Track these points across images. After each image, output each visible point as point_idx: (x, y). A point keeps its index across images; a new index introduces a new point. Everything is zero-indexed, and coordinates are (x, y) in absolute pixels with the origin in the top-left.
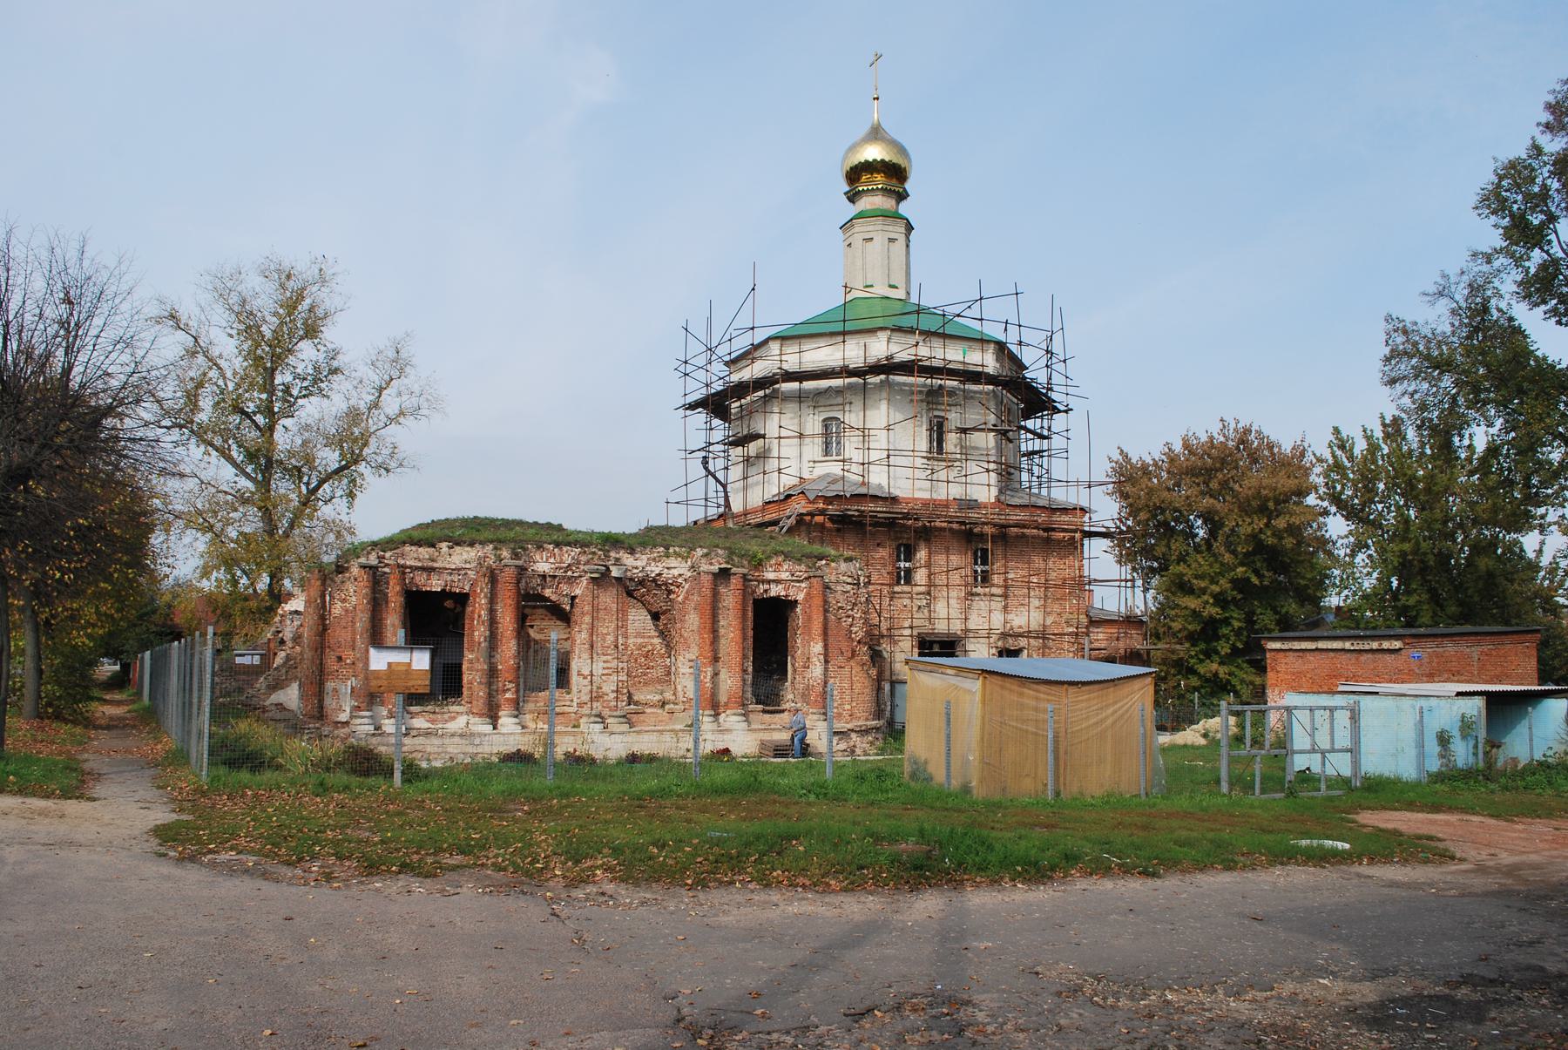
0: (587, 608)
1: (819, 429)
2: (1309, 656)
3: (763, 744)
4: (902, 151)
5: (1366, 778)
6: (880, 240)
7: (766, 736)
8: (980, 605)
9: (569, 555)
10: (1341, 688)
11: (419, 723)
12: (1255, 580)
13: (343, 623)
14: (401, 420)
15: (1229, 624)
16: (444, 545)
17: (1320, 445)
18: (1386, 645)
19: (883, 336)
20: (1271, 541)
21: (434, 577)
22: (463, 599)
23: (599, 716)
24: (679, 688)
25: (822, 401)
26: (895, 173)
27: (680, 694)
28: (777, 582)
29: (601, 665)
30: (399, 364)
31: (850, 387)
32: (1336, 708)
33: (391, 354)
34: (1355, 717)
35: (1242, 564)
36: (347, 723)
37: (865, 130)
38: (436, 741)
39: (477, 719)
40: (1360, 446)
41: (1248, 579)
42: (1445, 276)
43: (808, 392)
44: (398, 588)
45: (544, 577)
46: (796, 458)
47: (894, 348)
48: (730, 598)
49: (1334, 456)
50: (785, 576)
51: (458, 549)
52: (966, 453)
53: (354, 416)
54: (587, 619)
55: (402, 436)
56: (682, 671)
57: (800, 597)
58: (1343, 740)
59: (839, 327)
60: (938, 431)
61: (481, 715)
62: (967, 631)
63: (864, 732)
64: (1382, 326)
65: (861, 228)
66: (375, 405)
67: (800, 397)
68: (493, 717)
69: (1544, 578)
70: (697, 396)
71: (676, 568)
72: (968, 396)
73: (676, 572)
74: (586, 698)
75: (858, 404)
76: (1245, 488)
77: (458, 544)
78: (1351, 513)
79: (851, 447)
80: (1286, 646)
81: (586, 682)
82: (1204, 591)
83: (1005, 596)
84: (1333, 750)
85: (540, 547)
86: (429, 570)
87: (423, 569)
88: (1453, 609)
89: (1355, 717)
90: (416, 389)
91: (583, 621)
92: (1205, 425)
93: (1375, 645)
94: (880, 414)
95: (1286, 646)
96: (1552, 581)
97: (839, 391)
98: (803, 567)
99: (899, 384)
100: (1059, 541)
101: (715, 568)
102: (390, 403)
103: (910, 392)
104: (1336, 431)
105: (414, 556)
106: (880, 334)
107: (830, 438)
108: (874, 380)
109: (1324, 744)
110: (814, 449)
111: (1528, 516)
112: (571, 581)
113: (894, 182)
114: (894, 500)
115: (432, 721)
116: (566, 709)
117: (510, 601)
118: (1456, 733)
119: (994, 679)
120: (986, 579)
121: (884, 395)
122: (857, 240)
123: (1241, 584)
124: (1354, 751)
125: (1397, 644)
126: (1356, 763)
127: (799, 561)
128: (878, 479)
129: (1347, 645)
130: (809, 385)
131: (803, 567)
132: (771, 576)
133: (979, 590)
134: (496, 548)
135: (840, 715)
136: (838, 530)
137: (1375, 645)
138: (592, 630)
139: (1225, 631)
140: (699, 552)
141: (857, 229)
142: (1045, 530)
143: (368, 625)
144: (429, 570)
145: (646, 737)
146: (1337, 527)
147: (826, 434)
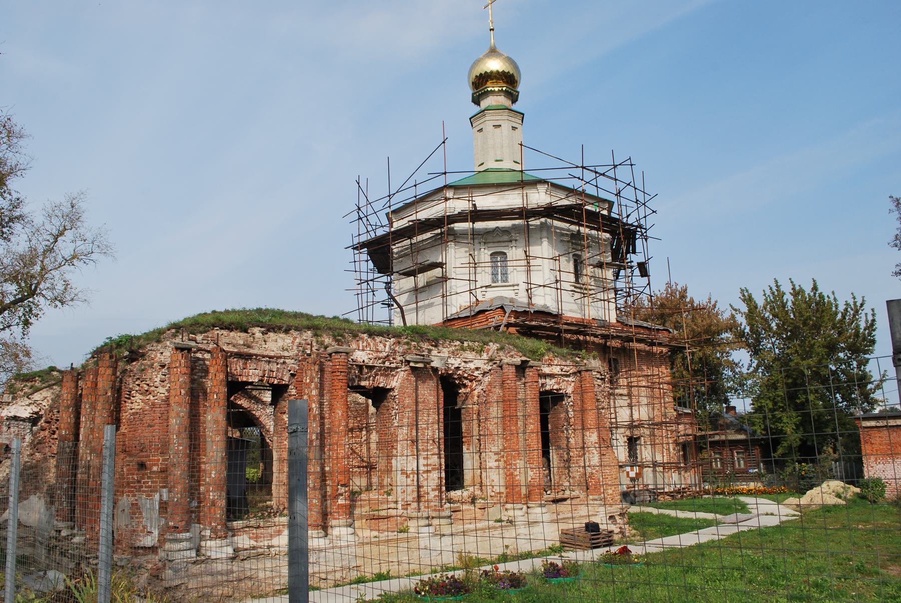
1: (488, 259)
3: (564, 533)
4: (519, 72)
6: (506, 126)
9: (385, 346)
11: (244, 541)
14: (75, 261)
16: (257, 331)
19: (542, 188)
21: (251, 365)
25: (490, 239)
26: (509, 80)
28: (552, 376)
30: (71, 218)
31: (514, 227)
33: (67, 209)
36: (153, 549)
37: (487, 50)
45: (360, 368)
46: (467, 279)
50: (556, 370)
51: (271, 334)
53: (28, 259)
55: (77, 276)
56: (489, 465)
57: (569, 390)
66: (49, 250)
67: (475, 235)
70: (363, 238)
73: (472, 366)
75: (522, 242)
79: (517, 276)
83: (629, 395)
90: (89, 236)
94: (543, 249)
97: (505, 231)
101: (518, 360)
102: (65, 247)
103: (561, 234)
105: (232, 340)
106: (539, 186)
108: (535, 222)
110: (484, 278)
112: (388, 372)
114: (557, 317)
115: (256, 538)
116: (393, 512)
121: (545, 234)
130: (479, 225)
132: (546, 370)
140: (493, 347)
141: (487, 118)
143: (186, 422)
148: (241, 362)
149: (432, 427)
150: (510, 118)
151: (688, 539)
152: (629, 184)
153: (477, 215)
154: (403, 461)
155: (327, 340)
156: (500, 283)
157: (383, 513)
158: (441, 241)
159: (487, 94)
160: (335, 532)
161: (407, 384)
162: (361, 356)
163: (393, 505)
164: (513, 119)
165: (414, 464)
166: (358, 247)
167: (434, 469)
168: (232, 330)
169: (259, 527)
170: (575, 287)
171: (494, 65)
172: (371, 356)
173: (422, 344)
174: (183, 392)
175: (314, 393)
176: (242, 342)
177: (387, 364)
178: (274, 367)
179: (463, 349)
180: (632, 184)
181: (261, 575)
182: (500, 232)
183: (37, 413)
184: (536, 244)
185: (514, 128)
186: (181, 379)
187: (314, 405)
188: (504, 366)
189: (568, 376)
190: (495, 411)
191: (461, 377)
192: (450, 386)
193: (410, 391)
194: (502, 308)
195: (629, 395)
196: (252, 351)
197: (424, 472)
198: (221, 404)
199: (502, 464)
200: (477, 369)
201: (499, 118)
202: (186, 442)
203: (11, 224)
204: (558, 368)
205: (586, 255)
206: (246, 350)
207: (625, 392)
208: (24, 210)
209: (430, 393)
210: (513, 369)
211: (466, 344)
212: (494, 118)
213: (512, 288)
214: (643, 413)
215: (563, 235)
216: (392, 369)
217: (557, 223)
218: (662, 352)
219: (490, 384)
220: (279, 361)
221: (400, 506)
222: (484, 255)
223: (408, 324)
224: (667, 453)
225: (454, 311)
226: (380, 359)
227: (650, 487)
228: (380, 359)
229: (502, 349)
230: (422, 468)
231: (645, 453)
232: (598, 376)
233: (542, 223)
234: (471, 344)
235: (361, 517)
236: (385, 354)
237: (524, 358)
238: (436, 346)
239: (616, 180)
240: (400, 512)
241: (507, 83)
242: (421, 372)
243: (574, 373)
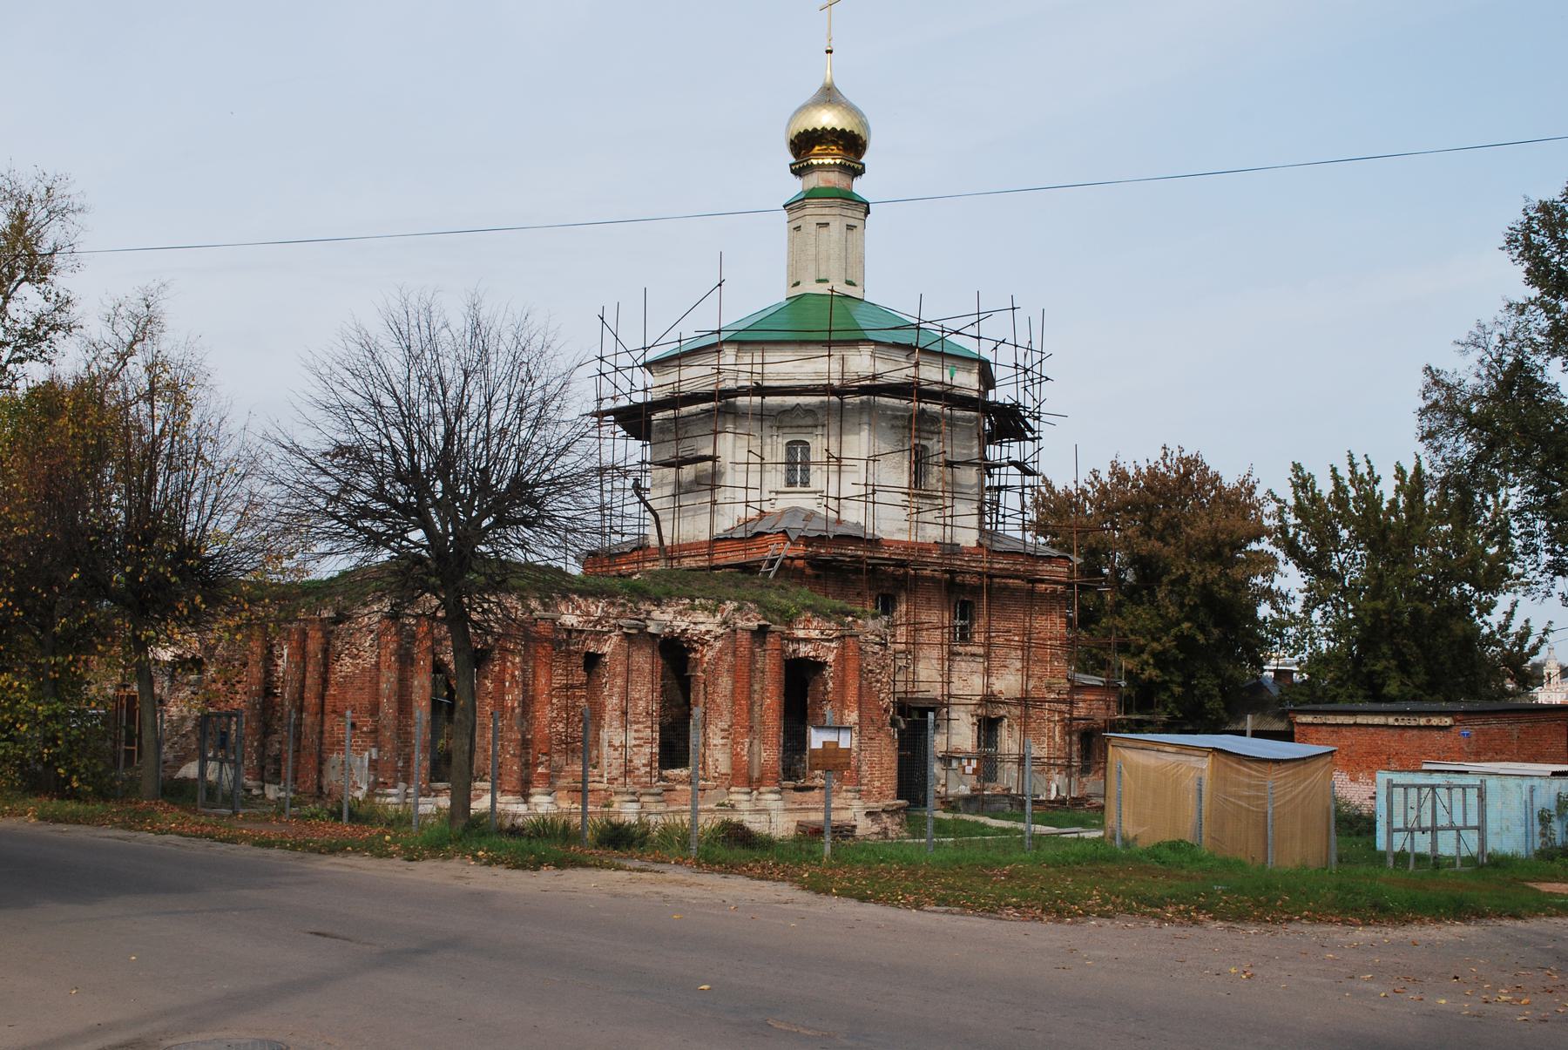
1: (781, 456)
2: (1346, 732)
3: (800, 825)
4: (865, 126)
5: (1489, 856)
6: (837, 226)
7: (802, 817)
8: (961, 666)
10: (1425, 767)
12: (1201, 638)
13: (358, 683)
15: (1167, 689)
17: (1274, 484)
18: (1435, 721)
19: (866, 351)
20: (1224, 593)
24: (710, 761)
26: (851, 144)
28: (807, 641)
29: (633, 734)
31: (822, 406)
32: (1468, 786)
34: (1482, 796)
35: (1187, 619)
37: (814, 89)
39: (510, 798)
40: (1325, 487)
41: (1194, 639)
42: (1481, 327)
43: (771, 409)
45: (569, 631)
46: (751, 485)
47: (881, 367)
49: (1297, 498)
50: (815, 634)
52: (955, 491)
57: (830, 658)
58: (1473, 820)
59: (825, 336)
60: (919, 463)
61: (514, 793)
62: (950, 696)
63: (892, 812)
64: (1421, 380)
65: (814, 213)
67: (762, 415)
69: (1514, 644)
71: (703, 623)
72: (952, 422)
73: (703, 628)
75: (834, 428)
76: (1199, 530)
78: (1304, 562)
80: (1318, 720)
82: (1141, 650)
83: (987, 656)
84: (1466, 828)
85: (565, 597)
88: (1422, 678)
89: (1482, 796)
92: (1141, 453)
93: (1423, 721)
94: (859, 443)
95: (1318, 720)
96: (1522, 648)
97: (809, 411)
98: (833, 624)
99: (887, 407)
100: (1042, 595)
101: (754, 624)
104: (1297, 468)
107: (797, 468)
109: (1459, 822)
110: (776, 478)
111: (1506, 573)
112: (599, 636)
113: (852, 156)
114: (875, 543)
118: (1554, 812)
119: (1221, 758)
120: (965, 638)
121: (865, 418)
122: (809, 224)
123: (1184, 642)
124: (1481, 829)
125: (1448, 721)
126: (1483, 841)
127: (827, 618)
128: (854, 514)
129: (1391, 721)
131: (833, 624)
132: (801, 634)
133: (961, 649)
136: (817, 577)
137: (1423, 721)
138: (625, 695)
139: (1164, 696)
140: (730, 606)
141: (807, 211)
142: (1029, 581)
143: (395, 687)
146: (1291, 580)
147: (791, 464)
149: (645, 696)
154: (611, 733)
155: (534, 604)
156: (798, 488)
160: (534, 800)
161: (619, 650)
162: (570, 619)
164: (850, 213)
165: (626, 739)
171: (827, 119)
173: (641, 605)
179: (694, 609)
182: (798, 418)
183: (179, 656)
184: (851, 432)
185: (850, 227)
190: (725, 683)
191: (689, 641)
192: (675, 655)
193: (622, 658)
194: (784, 532)
195: (987, 656)
199: (728, 741)
200: (708, 632)
201: (827, 211)
202: (395, 705)
203: (52, 334)
205: (934, 445)
207: (981, 651)
208: (75, 312)
209: (644, 660)
210: (748, 635)
212: (819, 211)
214: (1008, 683)
215: (896, 417)
219: (721, 650)
222: (776, 449)
223: (667, 542)
225: (728, 525)
227: (1014, 792)
229: (738, 609)
231: (1008, 742)
233: (862, 402)
238: (658, 606)
240: (604, 786)
241: (845, 149)
242: (636, 637)
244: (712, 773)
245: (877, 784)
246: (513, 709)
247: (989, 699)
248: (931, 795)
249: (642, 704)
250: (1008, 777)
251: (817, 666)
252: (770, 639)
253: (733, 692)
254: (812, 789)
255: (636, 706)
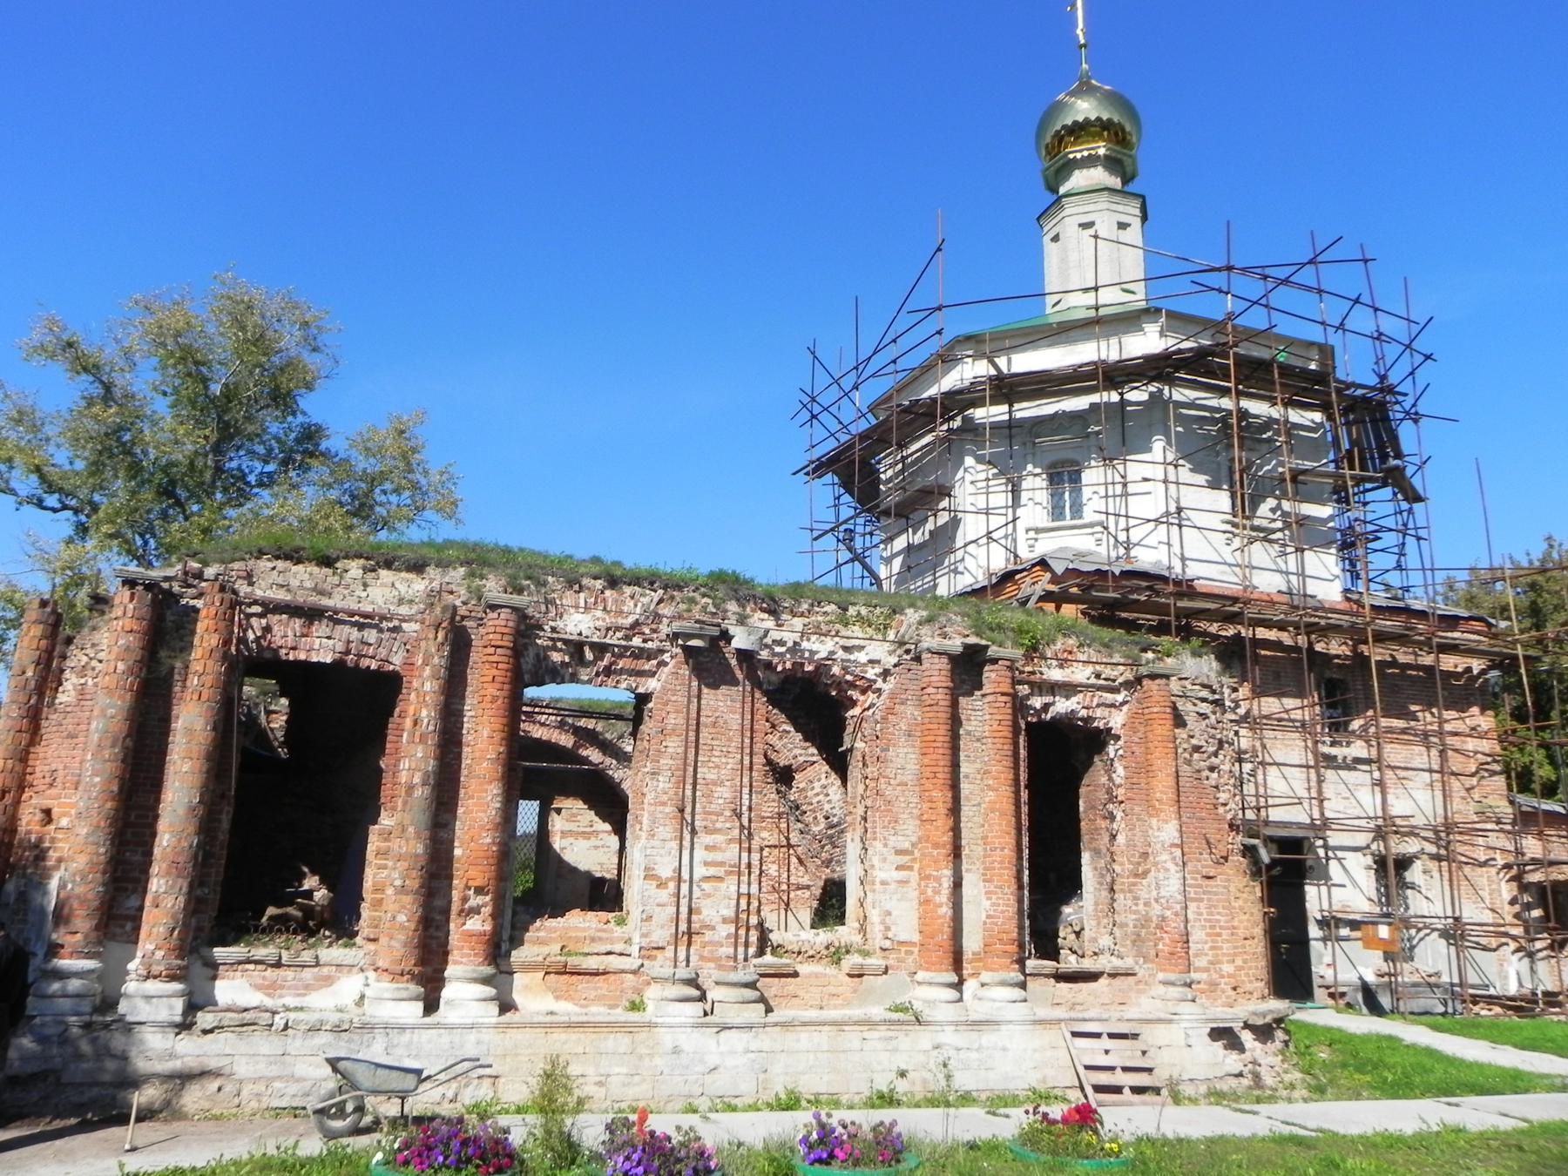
0: (675, 720)
9: (633, 604)
16: (355, 568)
21: (320, 628)
22: (382, 690)
23: (693, 982)
24: (874, 916)
27: (875, 930)
28: (1069, 689)
38: (264, 1044)
44: (214, 640)
48: (984, 717)
54: (674, 745)
57: (1117, 721)
68: (428, 972)
73: (862, 657)
74: (661, 935)
77: (388, 565)
81: (665, 895)
86: (311, 615)
87: (293, 610)
91: (648, 785)
101: (956, 644)
107: (1065, 506)
108: (1138, 395)
115: (271, 988)
116: (614, 962)
117: (492, 690)
130: (1027, 410)
132: (1055, 674)
134: (472, 575)
135: (1213, 985)
141: (1067, 212)
144: (311, 615)
145: (804, 1039)
148: (297, 623)
150: (1114, 207)
151: (1479, 1114)
152: (1357, 301)
153: (1007, 388)
156: (1068, 522)
157: (592, 963)
158: (952, 448)
159: (1069, 167)
163: (618, 948)
164: (1120, 208)
166: (820, 468)
167: (729, 873)
168: (299, 562)
169: (278, 965)
170: (1235, 525)
172: (599, 623)
174: (121, 666)
175: (427, 686)
176: (308, 584)
177: (637, 641)
178: (371, 635)
180: (1365, 299)
181: (242, 1069)
186: (121, 642)
187: (424, 713)
188: (924, 656)
189: (1115, 690)
191: (841, 685)
196: (326, 602)
197: (707, 879)
198: (205, 697)
199: (913, 876)
201: (1087, 208)
204: (1089, 670)
206: (314, 599)
210: (943, 664)
211: (852, 611)
212: (1081, 209)
213: (1089, 530)
214: (1416, 801)
216: (649, 655)
217: (1181, 394)
218: (1469, 670)
219: (893, 696)
220: (384, 624)
221: (635, 950)
224: (1490, 898)
226: (618, 629)
227: (1445, 979)
228: (618, 629)
230: (700, 871)
231: (1428, 895)
232: (1204, 693)
234: (864, 611)
235: (530, 967)
236: (631, 620)
237: (973, 640)
239: (1320, 291)
243: (1128, 685)
244: (877, 940)
245: (1227, 968)
246: (410, 788)
247: (1384, 829)
248: (1316, 981)
249: (724, 793)
250: (1433, 957)
251: (1092, 740)
252: (990, 675)
253: (920, 777)
254: (1092, 977)
255: (709, 796)
